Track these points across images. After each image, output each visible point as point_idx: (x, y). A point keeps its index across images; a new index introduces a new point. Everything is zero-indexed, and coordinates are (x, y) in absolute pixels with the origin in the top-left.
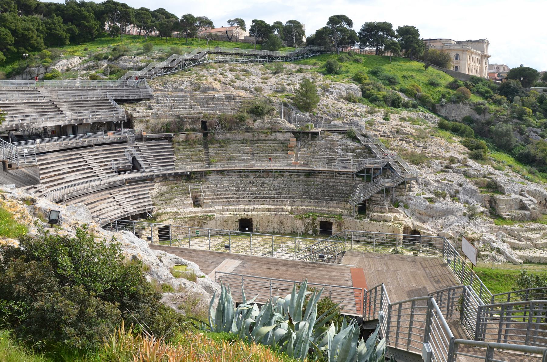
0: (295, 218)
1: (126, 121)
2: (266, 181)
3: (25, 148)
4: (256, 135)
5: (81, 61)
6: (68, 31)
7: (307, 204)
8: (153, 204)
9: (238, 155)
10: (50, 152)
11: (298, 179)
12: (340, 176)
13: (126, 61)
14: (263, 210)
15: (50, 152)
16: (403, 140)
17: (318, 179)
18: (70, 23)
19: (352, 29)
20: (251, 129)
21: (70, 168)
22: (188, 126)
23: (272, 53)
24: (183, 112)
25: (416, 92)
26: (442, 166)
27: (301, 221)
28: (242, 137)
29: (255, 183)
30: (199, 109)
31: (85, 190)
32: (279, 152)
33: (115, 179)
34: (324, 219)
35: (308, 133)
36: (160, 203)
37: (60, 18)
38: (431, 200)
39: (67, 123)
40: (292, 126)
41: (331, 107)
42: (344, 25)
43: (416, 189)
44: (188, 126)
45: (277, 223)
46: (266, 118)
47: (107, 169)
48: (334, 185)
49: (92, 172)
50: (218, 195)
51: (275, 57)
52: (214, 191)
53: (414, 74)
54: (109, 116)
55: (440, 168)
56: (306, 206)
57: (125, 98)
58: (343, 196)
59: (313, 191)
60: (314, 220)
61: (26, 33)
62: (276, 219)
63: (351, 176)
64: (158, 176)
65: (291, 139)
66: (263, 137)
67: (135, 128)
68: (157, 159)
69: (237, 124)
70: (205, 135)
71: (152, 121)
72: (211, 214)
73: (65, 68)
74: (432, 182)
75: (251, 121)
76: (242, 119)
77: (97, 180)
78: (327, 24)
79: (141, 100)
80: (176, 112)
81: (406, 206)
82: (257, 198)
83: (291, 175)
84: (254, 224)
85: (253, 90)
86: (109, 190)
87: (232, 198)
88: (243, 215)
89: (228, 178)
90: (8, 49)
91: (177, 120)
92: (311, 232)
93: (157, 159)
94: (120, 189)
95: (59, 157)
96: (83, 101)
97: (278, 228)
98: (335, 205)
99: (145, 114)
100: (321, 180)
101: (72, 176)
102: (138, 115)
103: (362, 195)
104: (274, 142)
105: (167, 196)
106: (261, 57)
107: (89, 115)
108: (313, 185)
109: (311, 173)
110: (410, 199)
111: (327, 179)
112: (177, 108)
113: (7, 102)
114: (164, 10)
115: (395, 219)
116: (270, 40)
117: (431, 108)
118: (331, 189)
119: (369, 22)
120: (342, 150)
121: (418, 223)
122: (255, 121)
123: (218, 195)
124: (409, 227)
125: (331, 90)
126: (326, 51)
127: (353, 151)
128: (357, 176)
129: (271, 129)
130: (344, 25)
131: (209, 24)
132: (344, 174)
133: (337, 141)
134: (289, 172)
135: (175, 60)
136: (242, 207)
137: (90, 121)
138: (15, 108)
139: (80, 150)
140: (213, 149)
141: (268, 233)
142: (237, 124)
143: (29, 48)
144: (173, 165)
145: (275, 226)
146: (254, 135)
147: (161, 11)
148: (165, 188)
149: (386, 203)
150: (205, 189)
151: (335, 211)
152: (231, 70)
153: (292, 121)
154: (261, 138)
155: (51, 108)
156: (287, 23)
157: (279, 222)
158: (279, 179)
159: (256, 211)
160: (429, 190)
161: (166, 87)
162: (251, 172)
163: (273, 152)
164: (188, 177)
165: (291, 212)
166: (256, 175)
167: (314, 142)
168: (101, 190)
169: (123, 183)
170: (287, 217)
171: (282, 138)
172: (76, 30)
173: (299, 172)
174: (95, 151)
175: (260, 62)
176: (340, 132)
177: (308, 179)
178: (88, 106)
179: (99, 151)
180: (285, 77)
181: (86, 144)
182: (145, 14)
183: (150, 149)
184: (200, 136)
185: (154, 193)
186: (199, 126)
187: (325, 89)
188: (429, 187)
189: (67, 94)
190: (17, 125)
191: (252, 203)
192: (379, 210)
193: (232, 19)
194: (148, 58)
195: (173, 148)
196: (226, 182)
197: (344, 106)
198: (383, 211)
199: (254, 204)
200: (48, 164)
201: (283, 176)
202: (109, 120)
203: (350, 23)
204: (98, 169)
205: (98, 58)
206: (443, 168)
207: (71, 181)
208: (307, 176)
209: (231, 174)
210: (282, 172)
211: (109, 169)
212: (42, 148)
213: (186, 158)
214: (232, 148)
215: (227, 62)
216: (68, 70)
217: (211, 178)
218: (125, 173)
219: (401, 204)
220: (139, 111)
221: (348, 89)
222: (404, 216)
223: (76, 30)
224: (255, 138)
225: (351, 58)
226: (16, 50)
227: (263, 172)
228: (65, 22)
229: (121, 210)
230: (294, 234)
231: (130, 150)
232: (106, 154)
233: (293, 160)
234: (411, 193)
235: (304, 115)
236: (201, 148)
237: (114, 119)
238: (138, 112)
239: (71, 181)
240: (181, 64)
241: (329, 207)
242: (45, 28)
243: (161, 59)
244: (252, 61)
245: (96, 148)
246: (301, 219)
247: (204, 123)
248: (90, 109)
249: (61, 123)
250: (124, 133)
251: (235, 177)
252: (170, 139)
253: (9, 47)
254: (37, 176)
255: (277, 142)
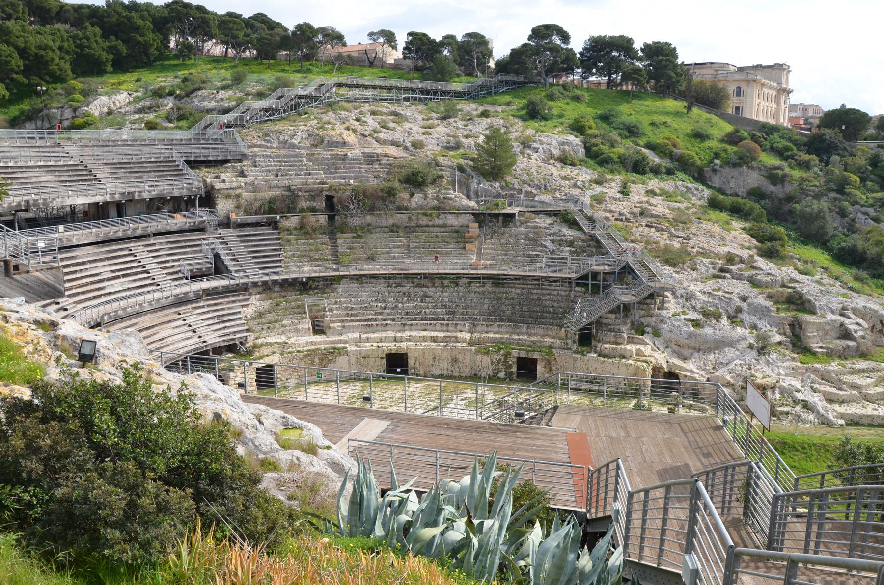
0: (477, 352)
1: (204, 196)
2: (431, 291)
3: (41, 240)
4: (413, 218)
5: (131, 99)
6: (110, 50)
7: (496, 329)
8: (248, 330)
9: (384, 251)
10: (81, 246)
11: (481, 289)
12: (550, 285)
13: (203, 99)
14: (424, 339)
15: (81, 246)
16: (651, 227)
17: (513, 290)
18: (113, 38)
19: (570, 46)
20: (406, 208)
21: (113, 271)
22: (303, 204)
23: (439, 86)
24: (295, 181)
25: (673, 149)
26: (714, 268)
27: (486, 357)
28: (391, 222)
29: (413, 295)
30: (321, 175)
31: (137, 307)
32: (451, 246)
33: (185, 289)
34: (523, 355)
35: (497, 216)
36: (259, 327)
37: (97, 30)
38: (696, 324)
39: (108, 198)
40: (472, 203)
41: (535, 173)
42: (557, 40)
43: (672, 306)
44: (303, 204)
45: (448, 360)
46: (431, 191)
47: (173, 273)
48: (539, 300)
49: (148, 278)
50: (352, 315)
51: (444, 93)
52: (346, 308)
53: (669, 120)
54: (177, 188)
55: (712, 271)
56: (495, 333)
57: (202, 158)
58: (554, 317)
59: (506, 309)
60: (507, 355)
61: (42, 53)
62: (445, 354)
63: (566, 284)
64: (255, 284)
65: (471, 225)
66: (425, 221)
67: (218, 207)
68: (254, 257)
69: (384, 200)
70: (331, 218)
71: (246, 195)
72: (341, 345)
73: (106, 110)
74: (698, 294)
75: (406, 196)
76: (391, 193)
77: (156, 291)
78: (529, 39)
79: (227, 161)
80: (285, 181)
81: (656, 334)
82: (415, 319)
83: (470, 283)
84: (411, 362)
85: (409, 145)
86: (177, 307)
87: (376, 320)
88: (392, 347)
89: (368, 287)
90: (12, 80)
91: (287, 193)
92: (502, 375)
93: (254, 257)
94: (194, 305)
95: (95, 254)
96: (134, 163)
97: (450, 368)
98: (541, 331)
99: (235, 184)
100: (518, 291)
101: (117, 285)
102: (223, 186)
103: (585, 315)
104: (443, 229)
105: (270, 317)
106: (422, 92)
107: (143, 187)
108: (506, 298)
109: (503, 279)
110: (662, 321)
111: (529, 289)
112: (287, 175)
113: (11, 164)
114: (266, 16)
115: (639, 353)
116: (437, 65)
117: (696, 175)
118: (536, 305)
119: (596, 35)
120: (553, 242)
121: (676, 361)
122: (412, 195)
123: (352, 315)
124: (661, 367)
125: (535, 145)
126: (527, 83)
127: (571, 244)
128: (578, 284)
129: (438, 208)
130: (557, 40)
131: (338, 38)
132: (556, 281)
133: (545, 228)
134: (467, 278)
135: (282, 97)
136: (391, 334)
137: (146, 196)
138: (24, 175)
139: (130, 243)
140: (344, 241)
141: (434, 376)
142: (384, 200)
143: (47, 78)
144: (280, 266)
145: (445, 365)
146: (410, 219)
147: (261, 18)
148: (267, 304)
149: (624, 328)
150: (331, 305)
151: (541, 342)
152: (374, 113)
153: (473, 196)
154: (421, 222)
155: (82, 175)
156: (463, 37)
157: (450, 359)
158: (452, 289)
159: (414, 341)
160: (694, 308)
161: (268, 141)
162: (405, 278)
163: (442, 245)
164: (304, 286)
165: (471, 343)
166: (413, 282)
167: (507, 230)
168: (163, 308)
169: (199, 296)
170: (464, 351)
171: (456, 224)
172: (124, 49)
173: (484, 279)
174: (154, 245)
175: (420, 99)
176: (549, 214)
177: (497, 289)
178: (142, 172)
179: (161, 244)
180: (460, 124)
181: (139, 232)
182: (235, 22)
183: (242, 241)
184: (323, 219)
185: (250, 311)
186: (321, 204)
187: (526, 144)
188: (693, 302)
189: (109, 151)
190: (27, 202)
191: (407, 327)
192: (613, 339)
193: (376, 31)
194: (239, 94)
195: (279, 239)
196: (365, 294)
197: (556, 171)
198: (619, 340)
199: (410, 330)
200: (77, 264)
201: (457, 285)
202: (176, 193)
203: (565, 37)
204: (158, 273)
205: (158, 94)
206: (715, 272)
207: (114, 293)
208: (497, 285)
209: (373, 280)
210: (455, 279)
211: (177, 273)
212: (68, 240)
213: (301, 256)
214: (374, 239)
215: (366, 100)
216: (110, 113)
217: (341, 287)
218: (202, 280)
219: (648, 329)
220: (225, 180)
221: (563, 144)
222: (652, 350)
223: (124, 49)
224: (413, 224)
225: (568, 93)
226: (25, 81)
227: (425, 278)
228: (105, 36)
229: (196, 340)
230: (475, 378)
231: (210, 242)
232: (171, 249)
233: (474, 258)
234: (664, 312)
235: (491, 186)
236: (325, 239)
237: (185, 193)
238: (224, 181)
239: (114, 293)
240: (293, 103)
241: (531, 335)
242: (73, 46)
243: (260, 95)
244: (407, 99)
245: (155, 239)
246: (487, 353)
247: (329, 199)
248: (146, 176)
249: (99, 199)
250: (201, 215)
251: (380, 286)
252: (274, 224)
253: (15, 76)
254: (60, 284)
255: (448, 229)
